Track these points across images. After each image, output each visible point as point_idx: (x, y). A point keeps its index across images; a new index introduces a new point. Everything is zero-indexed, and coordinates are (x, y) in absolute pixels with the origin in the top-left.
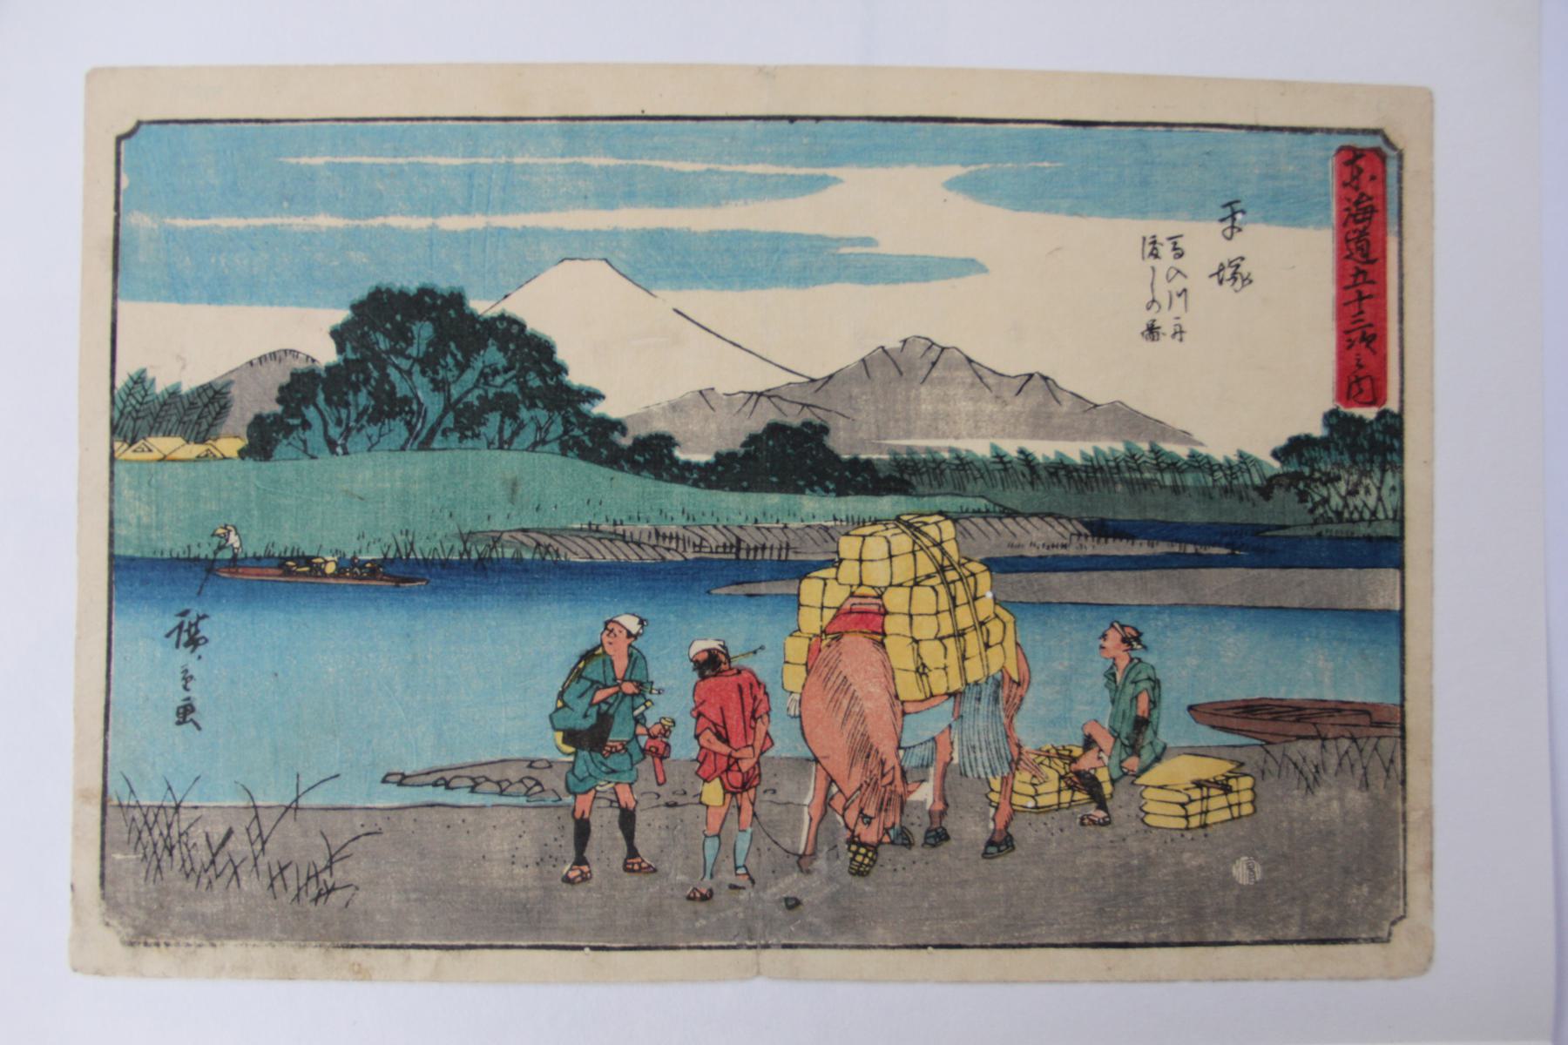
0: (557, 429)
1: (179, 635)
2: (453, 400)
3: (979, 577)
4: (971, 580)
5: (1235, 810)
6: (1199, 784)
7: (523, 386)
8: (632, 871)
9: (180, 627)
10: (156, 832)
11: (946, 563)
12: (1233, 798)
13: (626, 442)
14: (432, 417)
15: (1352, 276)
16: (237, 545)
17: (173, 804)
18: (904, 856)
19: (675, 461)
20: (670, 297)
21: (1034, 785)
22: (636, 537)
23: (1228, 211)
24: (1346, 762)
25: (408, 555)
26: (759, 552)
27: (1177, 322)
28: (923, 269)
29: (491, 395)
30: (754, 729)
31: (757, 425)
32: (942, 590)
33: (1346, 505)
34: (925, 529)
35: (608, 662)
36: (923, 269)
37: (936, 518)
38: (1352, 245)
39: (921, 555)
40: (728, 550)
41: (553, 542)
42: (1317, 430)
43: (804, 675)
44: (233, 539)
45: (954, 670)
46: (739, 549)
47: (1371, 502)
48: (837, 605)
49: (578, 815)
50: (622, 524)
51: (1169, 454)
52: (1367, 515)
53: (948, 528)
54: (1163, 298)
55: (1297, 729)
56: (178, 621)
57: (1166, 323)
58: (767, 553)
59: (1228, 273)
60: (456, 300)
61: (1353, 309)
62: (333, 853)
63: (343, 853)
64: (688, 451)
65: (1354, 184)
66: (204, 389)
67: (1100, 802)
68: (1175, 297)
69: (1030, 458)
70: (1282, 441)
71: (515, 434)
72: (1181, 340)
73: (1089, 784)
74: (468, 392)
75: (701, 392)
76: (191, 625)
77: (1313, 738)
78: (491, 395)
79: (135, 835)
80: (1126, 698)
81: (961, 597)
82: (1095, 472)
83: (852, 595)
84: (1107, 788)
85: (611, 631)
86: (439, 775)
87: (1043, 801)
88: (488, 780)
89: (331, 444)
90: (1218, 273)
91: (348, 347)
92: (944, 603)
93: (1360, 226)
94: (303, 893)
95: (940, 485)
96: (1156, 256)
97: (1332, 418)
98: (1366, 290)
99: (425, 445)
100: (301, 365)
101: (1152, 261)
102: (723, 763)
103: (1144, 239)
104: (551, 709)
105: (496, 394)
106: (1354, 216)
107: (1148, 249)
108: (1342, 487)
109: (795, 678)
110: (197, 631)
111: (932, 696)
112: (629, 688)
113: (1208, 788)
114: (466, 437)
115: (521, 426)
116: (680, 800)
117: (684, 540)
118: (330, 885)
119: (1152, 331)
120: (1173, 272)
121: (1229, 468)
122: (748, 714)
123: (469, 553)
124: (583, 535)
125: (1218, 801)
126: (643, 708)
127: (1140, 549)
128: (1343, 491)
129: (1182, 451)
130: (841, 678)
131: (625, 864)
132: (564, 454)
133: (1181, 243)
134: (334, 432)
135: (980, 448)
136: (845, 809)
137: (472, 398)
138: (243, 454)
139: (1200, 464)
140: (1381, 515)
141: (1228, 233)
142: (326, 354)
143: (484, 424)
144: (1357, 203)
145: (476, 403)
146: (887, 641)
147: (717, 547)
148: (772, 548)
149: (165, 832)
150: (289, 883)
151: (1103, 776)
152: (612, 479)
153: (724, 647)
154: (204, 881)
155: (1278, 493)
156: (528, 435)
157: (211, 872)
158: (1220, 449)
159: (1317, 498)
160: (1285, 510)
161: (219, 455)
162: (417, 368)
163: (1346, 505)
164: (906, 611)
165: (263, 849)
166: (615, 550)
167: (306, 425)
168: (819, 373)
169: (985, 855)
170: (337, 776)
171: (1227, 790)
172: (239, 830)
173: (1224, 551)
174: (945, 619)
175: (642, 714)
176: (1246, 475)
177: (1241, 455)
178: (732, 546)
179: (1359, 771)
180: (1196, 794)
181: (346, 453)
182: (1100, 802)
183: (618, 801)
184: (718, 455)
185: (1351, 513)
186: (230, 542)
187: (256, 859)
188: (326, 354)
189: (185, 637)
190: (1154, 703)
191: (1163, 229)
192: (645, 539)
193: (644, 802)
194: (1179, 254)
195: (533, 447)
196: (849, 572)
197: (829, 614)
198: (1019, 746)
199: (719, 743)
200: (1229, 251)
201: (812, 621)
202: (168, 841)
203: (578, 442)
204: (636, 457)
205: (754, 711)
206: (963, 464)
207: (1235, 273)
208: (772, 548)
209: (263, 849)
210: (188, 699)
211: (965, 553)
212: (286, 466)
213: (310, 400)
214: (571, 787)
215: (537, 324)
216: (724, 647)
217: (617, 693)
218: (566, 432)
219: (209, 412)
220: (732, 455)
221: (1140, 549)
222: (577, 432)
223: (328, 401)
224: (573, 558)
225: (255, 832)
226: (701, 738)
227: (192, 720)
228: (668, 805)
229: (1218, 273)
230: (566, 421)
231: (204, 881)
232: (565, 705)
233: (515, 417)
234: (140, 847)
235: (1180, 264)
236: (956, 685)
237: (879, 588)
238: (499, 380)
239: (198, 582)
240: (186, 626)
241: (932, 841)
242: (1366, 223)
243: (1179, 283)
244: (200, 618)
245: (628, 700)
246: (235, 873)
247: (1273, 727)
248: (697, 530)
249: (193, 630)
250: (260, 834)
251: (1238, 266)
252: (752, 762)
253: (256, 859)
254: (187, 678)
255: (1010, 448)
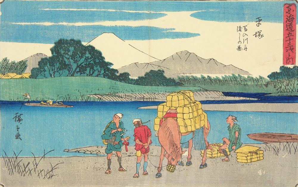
0: (103, 72)
1: (16, 119)
2: (79, 65)
3: (199, 105)
4: (197, 105)
5: (259, 158)
6: (250, 152)
7: (95, 62)
8: (121, 171)
9: (16, 117)
10: (12, 163)
11: (191, 102)
12: (258, 156)
13: (118, 74)
14: (74, 69)
15: (288, 34)
16: (29, 98)
17: (15, 157)
18: (182, 168)
19: (129, 79)
20: (128, 42)
21: (211, 152)
22: (121, 96)
23: (258, 20)
24: (285, 148)
25: (69, 100)
26: (147, 99)
27: (245, 46)
28: (188, 35)
29: (87, 64)
30: (148, 139)
31: (148, 71)
32: (190, 107)
33: (286, 88)
34: (186, 94)
35: (115, 124)
36: (188, 35)
37: (190, 91)
38: (288, 27)
39: (185, 100)
40: (142, 99)
41: (102, 97)
42: (279, 71)
43: (159, 127)
44: (28, 97)
45: (193, 126)
46: (144, 99)
47: (292, 87)
48: (166, 111)
49: (108, 159)
50: (117, 93)
51: (243, 77)
52: (291, 90)
53: (191, 94)
54: (242, 41)
55: (274, 140)
56: (15, 116)
57: (243, 47)
58: (150, 99)
59: (258, 34)
60: (79, 42)
61: (288, 42)
62: (53, 166)
63: (56, 167)
64: (133, 77)
65: (289, 12)
66: (20, 62)
67: (227, 156)
68: (245, 40)
69: (210, 78)
70: (270, 73)
71: (93, 73)
72: (246, 50)
73: (224, 152)
74: (82, 63)
75: (135, 63)
76: (18, 116)
77: (277, 142)
78: (87, 64)
79: (7, 164)
80: (233, 133)
81: (195, 110)
82: (226, 81)
83: (170, 109)
84: (228, 153)
85: (115, 117)
86: (77, 150)
87: (214, 156)
88: (88, 151)
89: (51, 76)
90: (255, 34)
91: (54, 53)
92: (191, 111)
93: (290, 22)
94: (46, 177)
95: (190, 84)
96: (241, 31)
97: (282, 68)
98: (291, 37)
99: (72, 75)
100: (44, 57)
101: (239, 32)
102: (141, 147)
103: (238, 27)
104: (102, 134)
105: (88, 64)
106: (289, 20)
107: (239, 29)
108: (285, 84)
109: (157, 128)
110: (20, 118)
111: (188, 132)
112: (119, 130)
113: (252, 153)
114: (82, 73)
115: (95, 71)
116: (132, 155)
117: (132, 97)
118: (52, 175)
119: (239, 48)
120: (244, 34)
121: (257, 80)
122: (146, 135)
123: (83, 100)
124: (109, 95)
125: (255, 156)
126: (123, 134)
127: (237, 98)
128: (285, 84)
129: (246, 76)
130: (167, 128)
131: (119, 169)
132: (104, 77)
133: (246, 28)
134: (52, 72)
135: (199, 76)
136: (168, 157)
137: (83, 64)
138: (31, 77)
139: (251, 79)
140: (294, 90)
141: (258, 25)
142: (49, 54)
143: (86, 71)
144: (289, 17)
145: (84, 65)
146: (177, 119)
147: (139, 98)
148: (152, 98)
149: (14, 164)
150: (42, 174)
151: (227, 150)
152: (115, 83)
153: (141, 121)
154: (23, 174)
155: (269, 86)
156: (96, 73)
157: (25, 172)
158: (255, 76)
159: (279, 87)
160: (271, 90)
161: (25, 77)
162: (70, 58)
163: (286, 88)
164: (182, 112)
165: (37, 167)
166: (113, 98)
167: (45, 71)
168: (162, 59)
169: (200, 168)
170: (54, 150)
171: (257, 154)
172: (31, 163)
173: (256, 99)
174: (191, 114)
175: (122, 135)
176: (262, 82)
177: (260, 77)
178: (142, 98)
179: (289, 150)
180: (249, 154)
181: (54, 77)
182: (227, 156)
183: (117, 155)
184: (139, 77)
185: (287, 90)
186: (28, 97)
187: (35, 169)
188: (49, 54)
189: (17, 119)
190: (239, 134)
191: (242, 24)
192: (123, 96)
193: (123, 156)
194: (246, 30)
195: (97, 76)
196: (169, 104)
197: (165, 113)
198: (208, 143)
199: (140, 142)
200: (258, 29)
201: (160, 115)
202: (14, 166)
203: (107, 75)
204: (121, 78)
205: (148, 135)
206: (195, 79)
207: (259, 34)
208: (152, 98)
209: (37, 167)
210: (18, 133)
211: (195, 100)
212: (40, 81)
213: (45, 64)
214: (106, 152)
215: (97, 48)
216: (141, 121)
217: (117, 131)
218: (105, 72)
219: (22, 67)
220: (142, 78)
221: (237, 98)
222: (107, 72)
223: (50, 65)
224: (106, 100)
225: (35, 163)
226: (136, 141)
227: (19, 138)
228: (129, 156)
229: (255, 35)
230: (104, 70)
231: (23, 174)
232: (105, 134)
233: (93, 69)
234: (8, 167)
235: (246, 32)
236: (194, 129)
237: (176, 107)
238: (89, 60)
239: (21, 106)
240: (17, 117)
241: (188, 164)
242: (292, 22)
243: (246, 37)
244: (21, 115)
245: (119, 133)
246: (30, 172)
247: (268, 139)
248: (135, 95)
249: (19, 117)
250: (36, 164)
251: (260, 33)
252: (147, 147)
253: (35, 169)
254: (18, 128)
255: (206, 76)
